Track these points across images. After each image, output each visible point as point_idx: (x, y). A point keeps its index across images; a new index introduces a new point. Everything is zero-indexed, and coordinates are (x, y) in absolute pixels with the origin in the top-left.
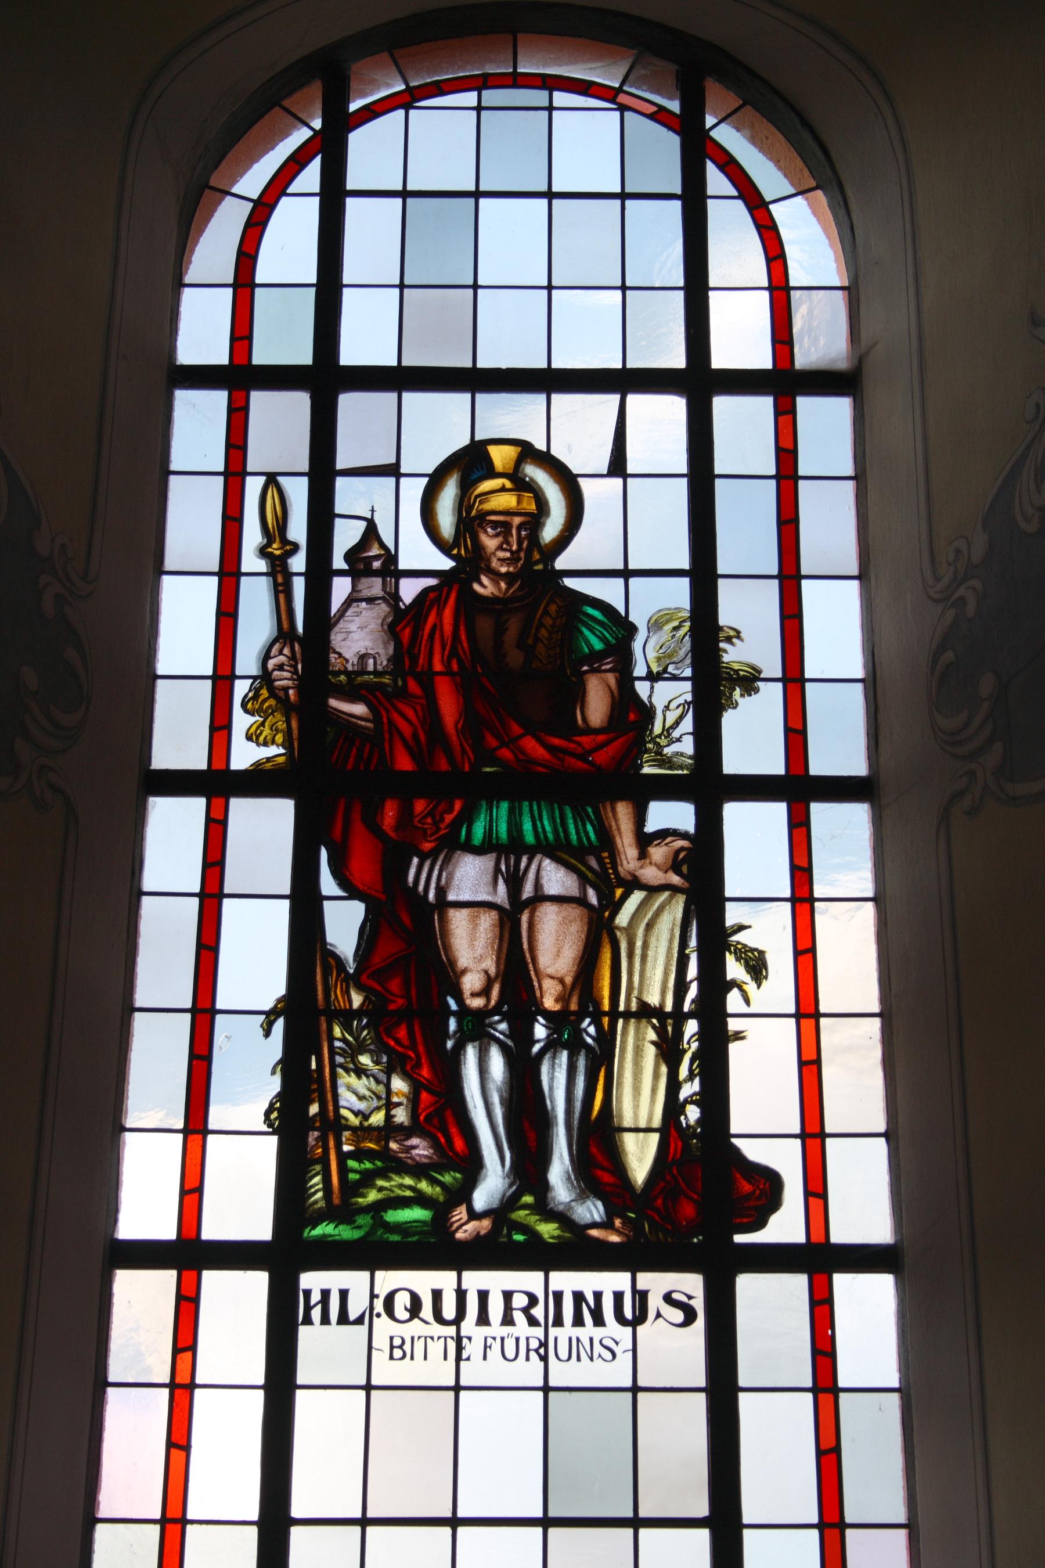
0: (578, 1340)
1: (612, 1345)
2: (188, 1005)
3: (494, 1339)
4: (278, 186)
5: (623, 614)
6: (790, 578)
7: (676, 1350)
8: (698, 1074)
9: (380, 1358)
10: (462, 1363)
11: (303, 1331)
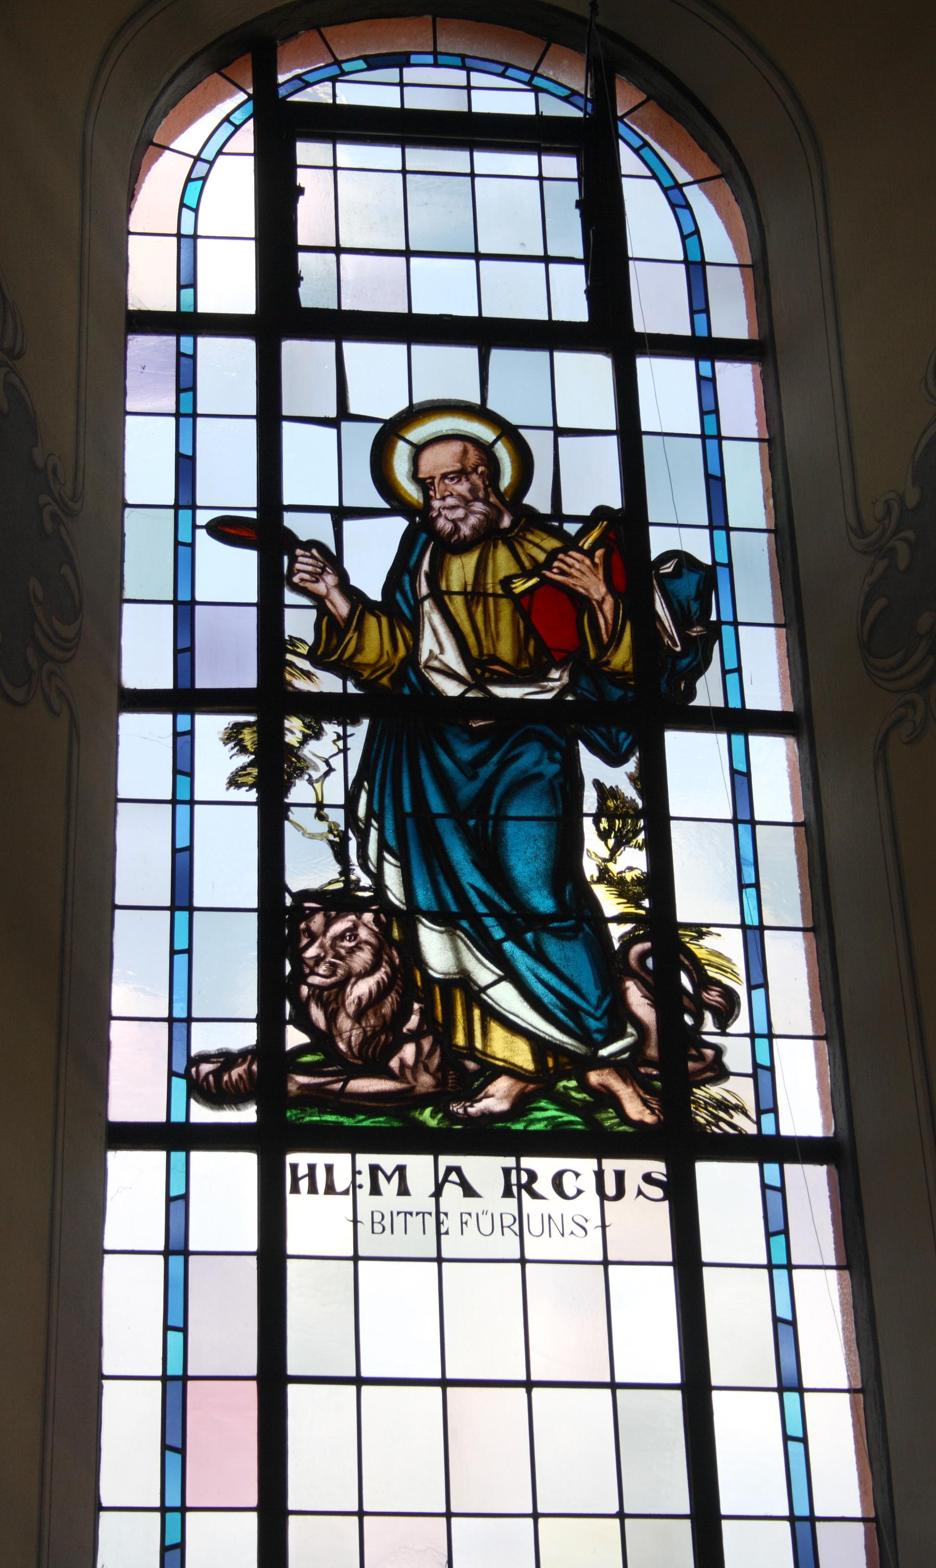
0: (550, 1217)
1: (583, 1223)
3: (470, 1214)
6: (711, 437)
7: (645, 1223)
8: (644, 828)
9: (364, 1229)
10: (443, 1237)
11: (291, 1199)
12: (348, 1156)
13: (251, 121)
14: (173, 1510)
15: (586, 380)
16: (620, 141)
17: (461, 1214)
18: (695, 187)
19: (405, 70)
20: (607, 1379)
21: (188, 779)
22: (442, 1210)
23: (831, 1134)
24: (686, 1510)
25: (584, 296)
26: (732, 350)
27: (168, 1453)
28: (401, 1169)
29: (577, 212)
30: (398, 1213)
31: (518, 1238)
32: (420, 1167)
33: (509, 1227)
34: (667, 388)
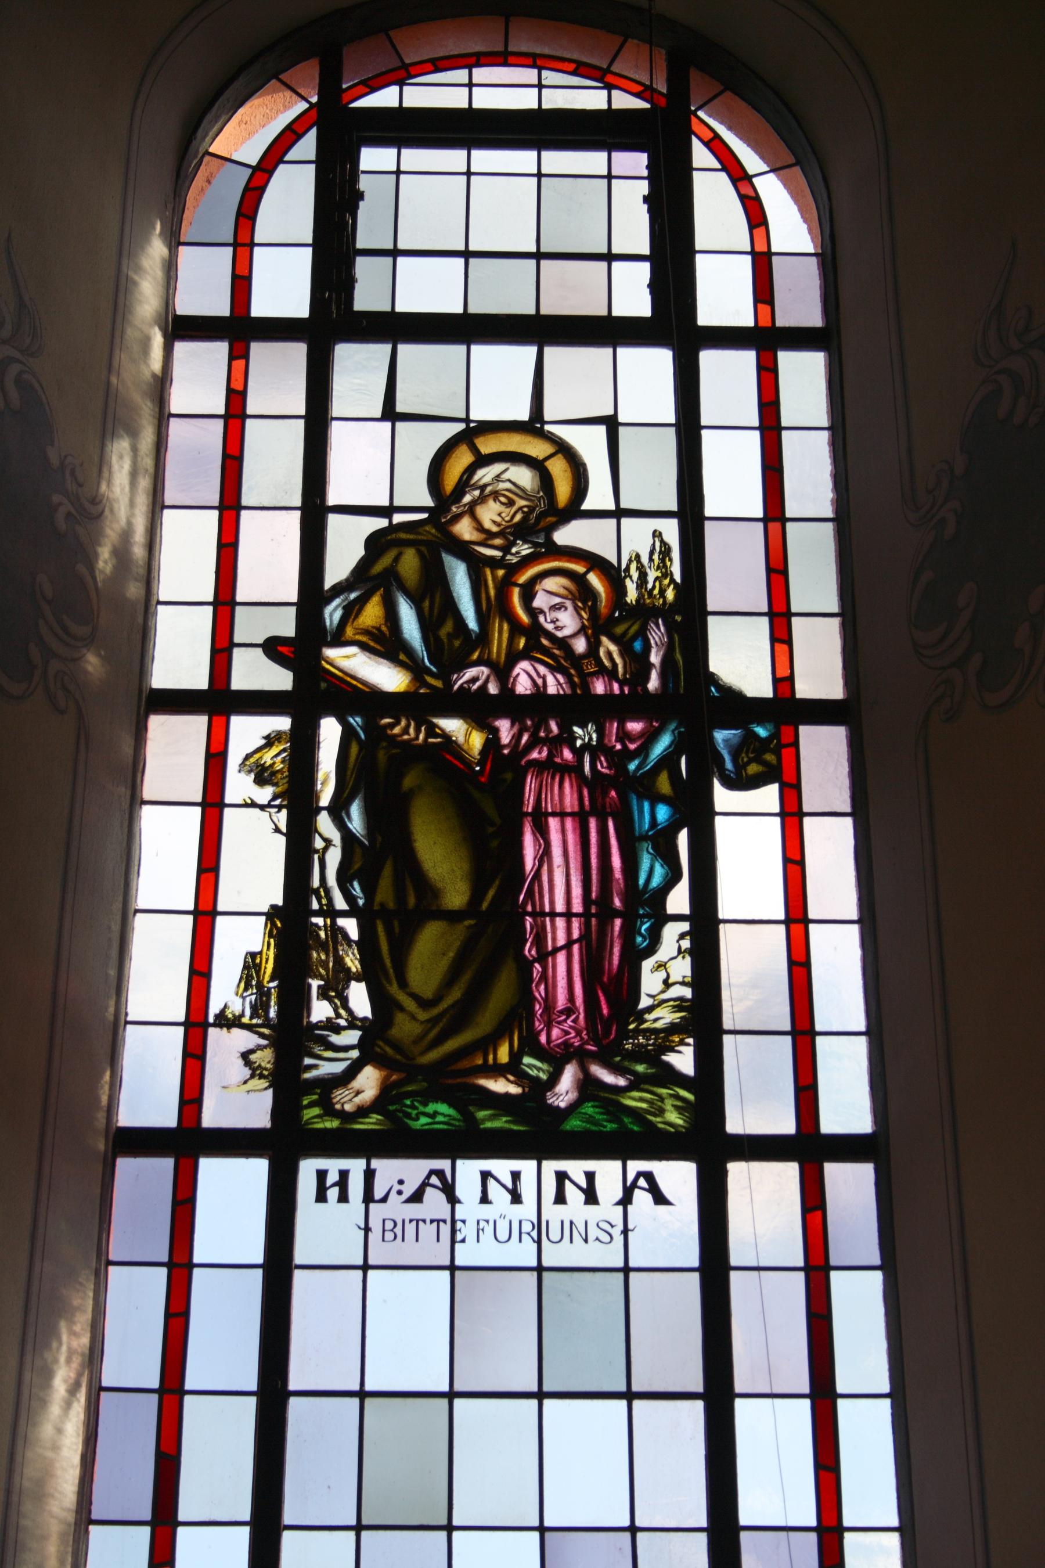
1: (607, 1227)
2: (191, 907)
3: (487, 1221)
4: (275, 155)
5: (616, 564)
9: (375, 1237)
10: (457, 1246)
15: (647, 375)
16: (694, 138)
17: (384, 1221)
25: (648, 291)
26: (800, 339)
28: (590, 1176)
29: (646, 207)
30: (411, 1221)
32: (609, 1173)
33: (529, 1234)
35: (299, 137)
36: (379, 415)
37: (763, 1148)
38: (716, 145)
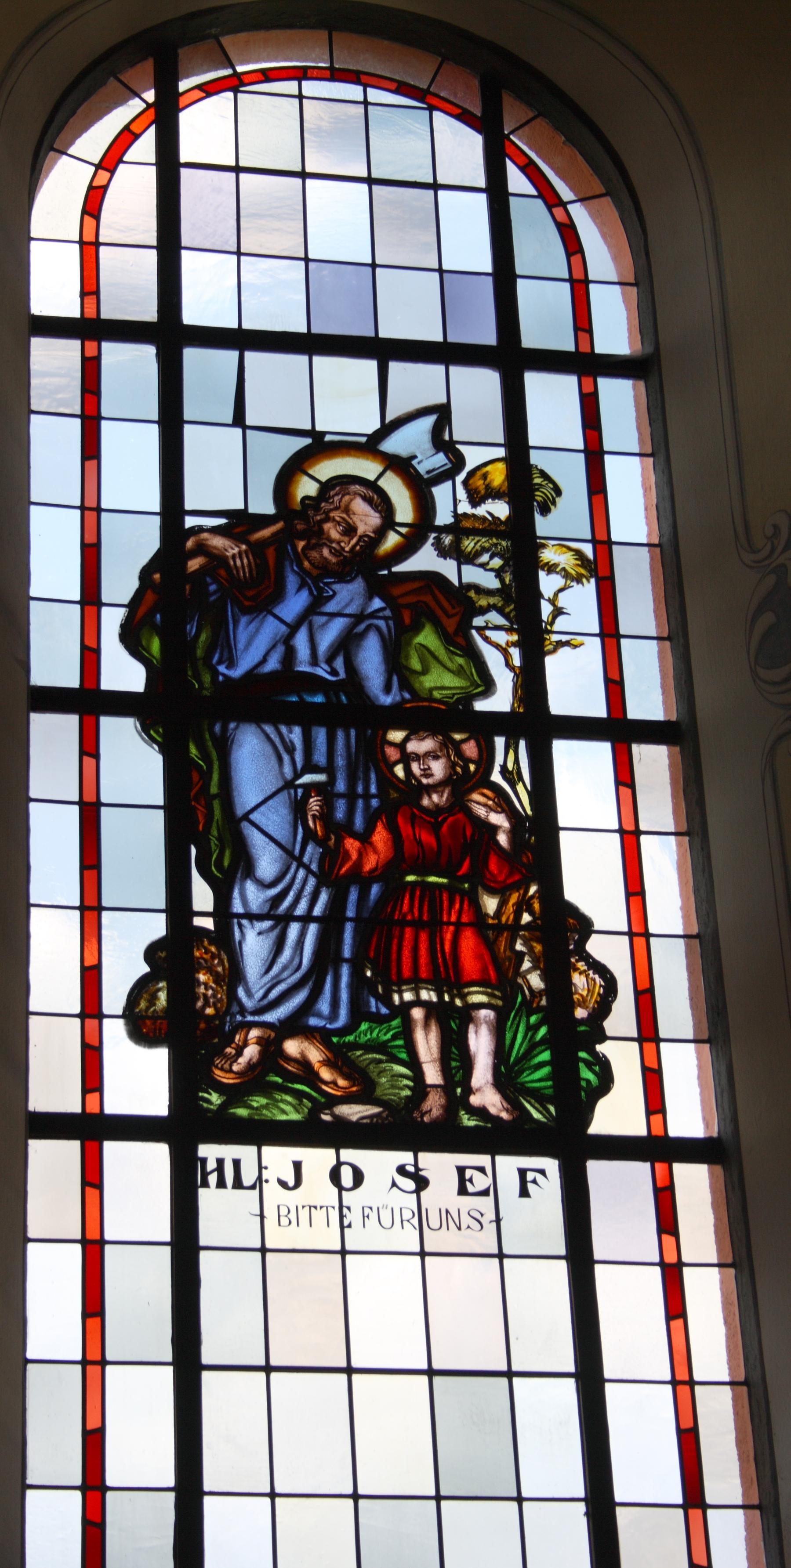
0: (447, 1212)
1: (478, 1216)
3: (371, 1208)
7: (540, 1215)
10: (346, 1230)
11: (202, 1191)
12: (254, 1149)
13: (154, 126)
14: (94, 1362)
18: (578, 204)
19: (304, 83)
20: (504, 1368)
21: (97, 1192)
22: (345, 1203)
23: (715, 1135)
24: (582, 1494)
26: (615, 367)
27: (88, 1189)
31: (417, 1232)
33: (408, 1221)
34: (552, 403)
35: (136, 137)
36: (230, 421)
37: (580, 728)
38: (530, 170)
